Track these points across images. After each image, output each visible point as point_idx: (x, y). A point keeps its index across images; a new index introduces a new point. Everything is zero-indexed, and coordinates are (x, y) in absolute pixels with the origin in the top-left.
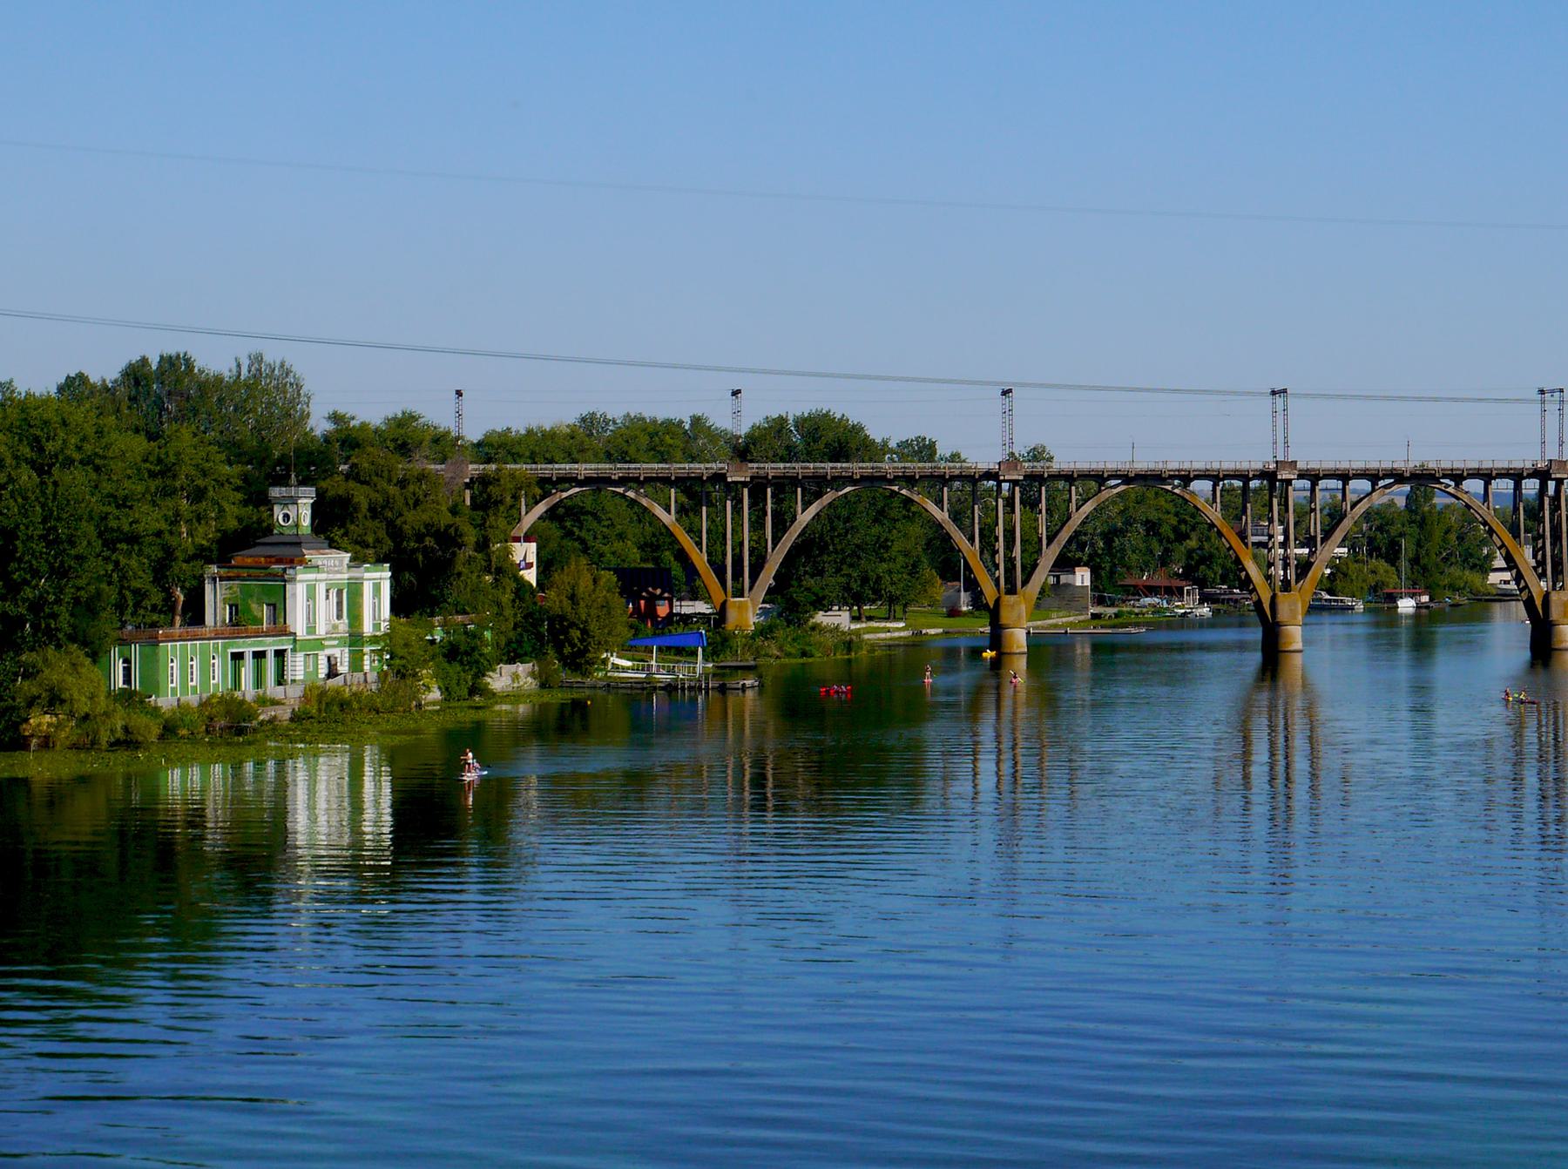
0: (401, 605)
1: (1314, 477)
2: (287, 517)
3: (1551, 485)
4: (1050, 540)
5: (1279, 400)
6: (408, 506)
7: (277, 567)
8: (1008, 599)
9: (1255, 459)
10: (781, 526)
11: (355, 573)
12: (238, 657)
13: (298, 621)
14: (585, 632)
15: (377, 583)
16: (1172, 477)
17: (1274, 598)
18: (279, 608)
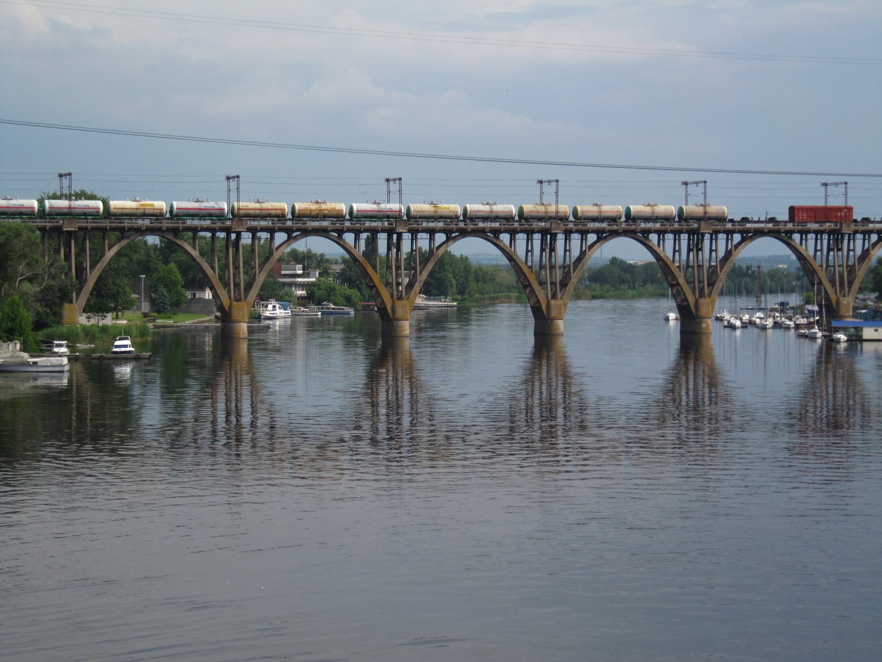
3: (233, 236)
5: (233, 184)
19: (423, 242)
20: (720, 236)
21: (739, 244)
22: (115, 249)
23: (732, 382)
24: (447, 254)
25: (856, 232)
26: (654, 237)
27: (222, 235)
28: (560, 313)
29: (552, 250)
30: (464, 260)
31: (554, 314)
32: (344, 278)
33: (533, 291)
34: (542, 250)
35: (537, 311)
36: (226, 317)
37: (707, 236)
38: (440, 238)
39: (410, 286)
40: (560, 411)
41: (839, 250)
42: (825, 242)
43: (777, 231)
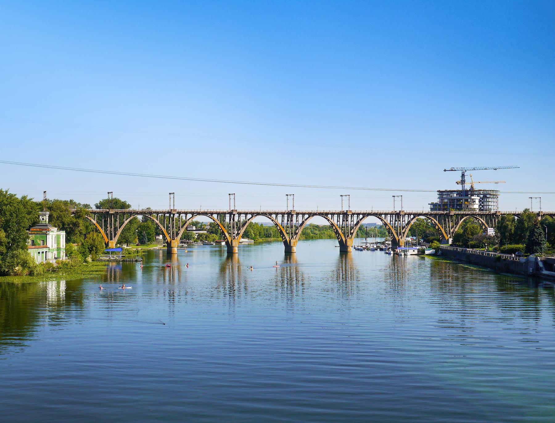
0: (68, 241)
1: (179, 213)
2: (43, 219)
3: (172, 215)
4: (182, 227)
5: (172, 196)
6: (68, 218)
7: (44, 231)
8: (173, 241)
9: (166, 208)
10: (121, 224)
11: (59, 233)
12: (39, 253)
13: (49, 245)
14: (96, 248)
15: (63, 234)
16: (154, 213)
17: (346, 240)
18: (45, 241)
19: (243, 218)
20: (355, 215)
21: (362, 218)
22: (463, 220)
23: (58, 291)
24: (251, 223)
25: (405, 214)
26: (330, 216)
27: (168, 215)
28: (294, 245)
29: (292, 221)
30: (256, 224)
31: (292, 245)
32: (211, 232)
33: (284, 235)
34: (288, 221)
35: (285, 243)
36: (169, 245)
37: (350, 216)
38: (249, 216)
39: (238, 234)
40: (294, 282)
41: (399, 221)
42: (394, 218)
43: (324, 215)
